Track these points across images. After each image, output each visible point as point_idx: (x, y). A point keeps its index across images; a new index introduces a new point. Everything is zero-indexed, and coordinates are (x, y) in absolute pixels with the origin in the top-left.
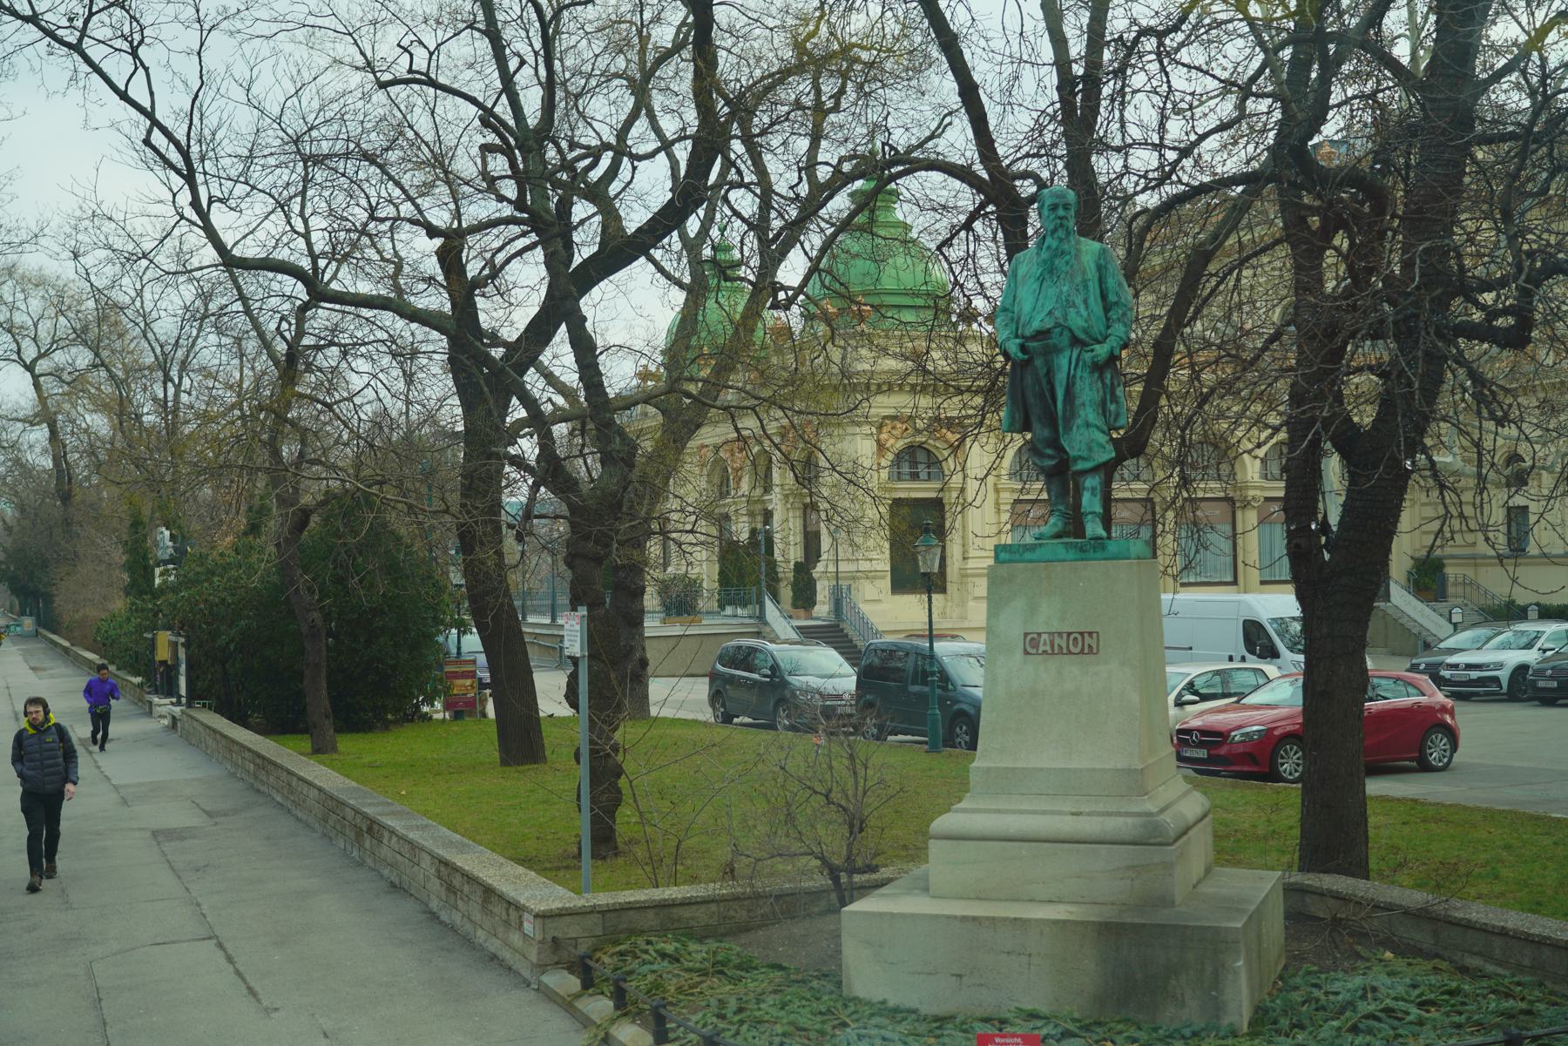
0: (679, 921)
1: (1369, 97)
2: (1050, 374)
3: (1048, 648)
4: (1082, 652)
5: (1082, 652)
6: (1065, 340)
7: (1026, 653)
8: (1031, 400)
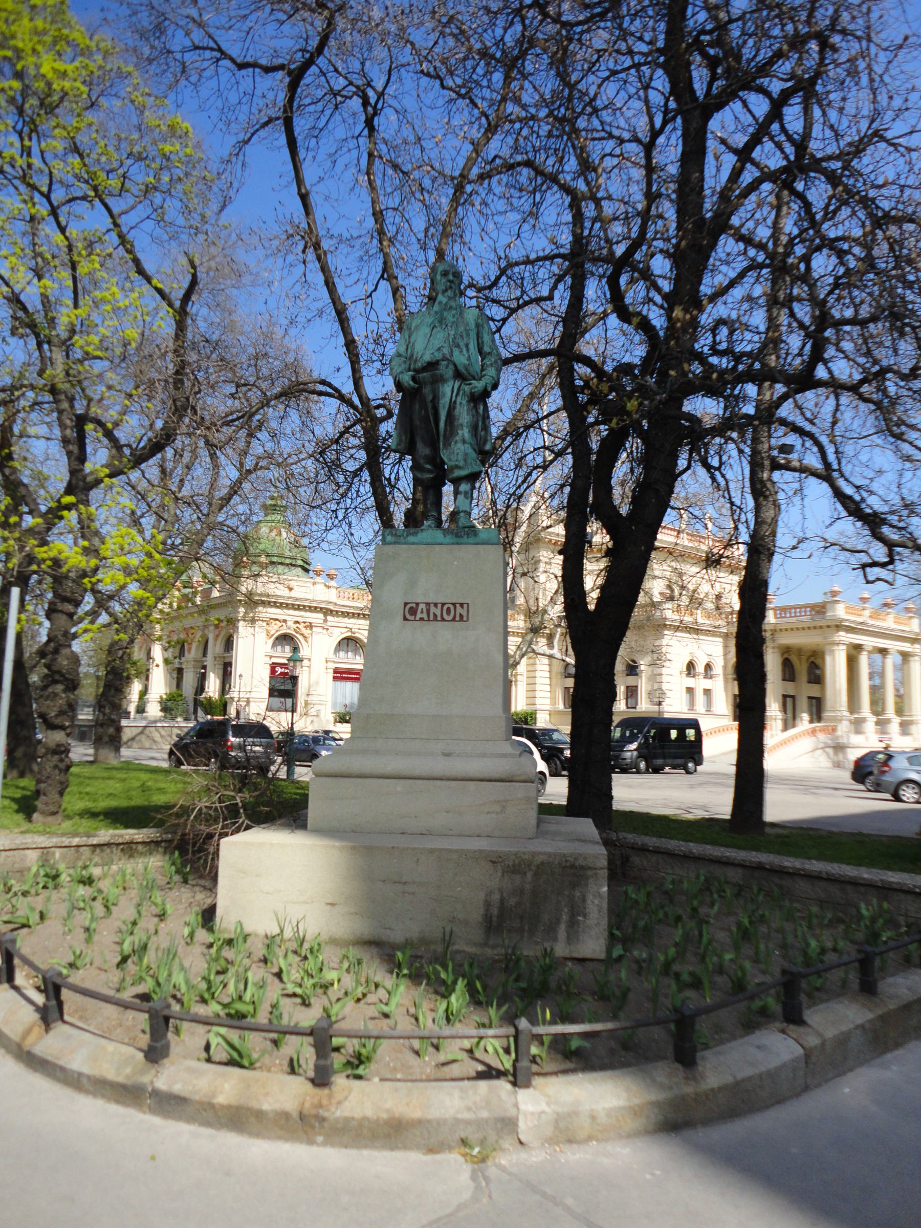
3: (425, 616)
4: (454, 620)
5: (454, 620)
6: (450, 372)
7: (405, 619)
8: (417, 422)
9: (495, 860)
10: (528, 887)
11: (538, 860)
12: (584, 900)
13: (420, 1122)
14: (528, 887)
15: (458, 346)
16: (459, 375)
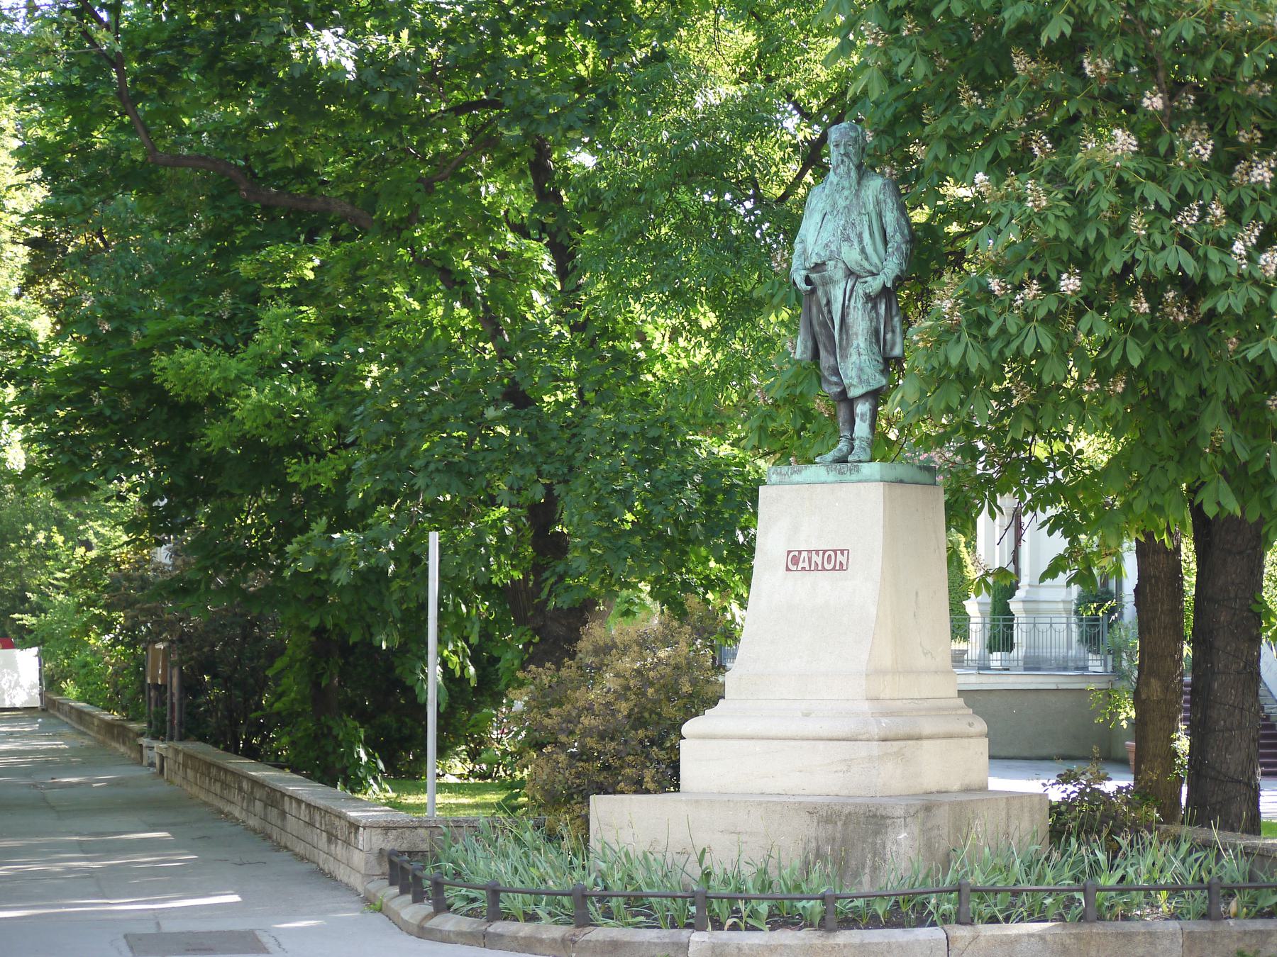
0: (1257, 602)
1: (264, 450)
4: (834, 569)
5: (834, 569)
6: (839, 274)
7: (788, 569)
8: (817, 328)
9: (812, 811)
10: (838, 835)
11: (847, 810)
12: (884, 848)
13: (628, 943)
14: (838, 835)
15: (848, 239)
16: (850, 273)
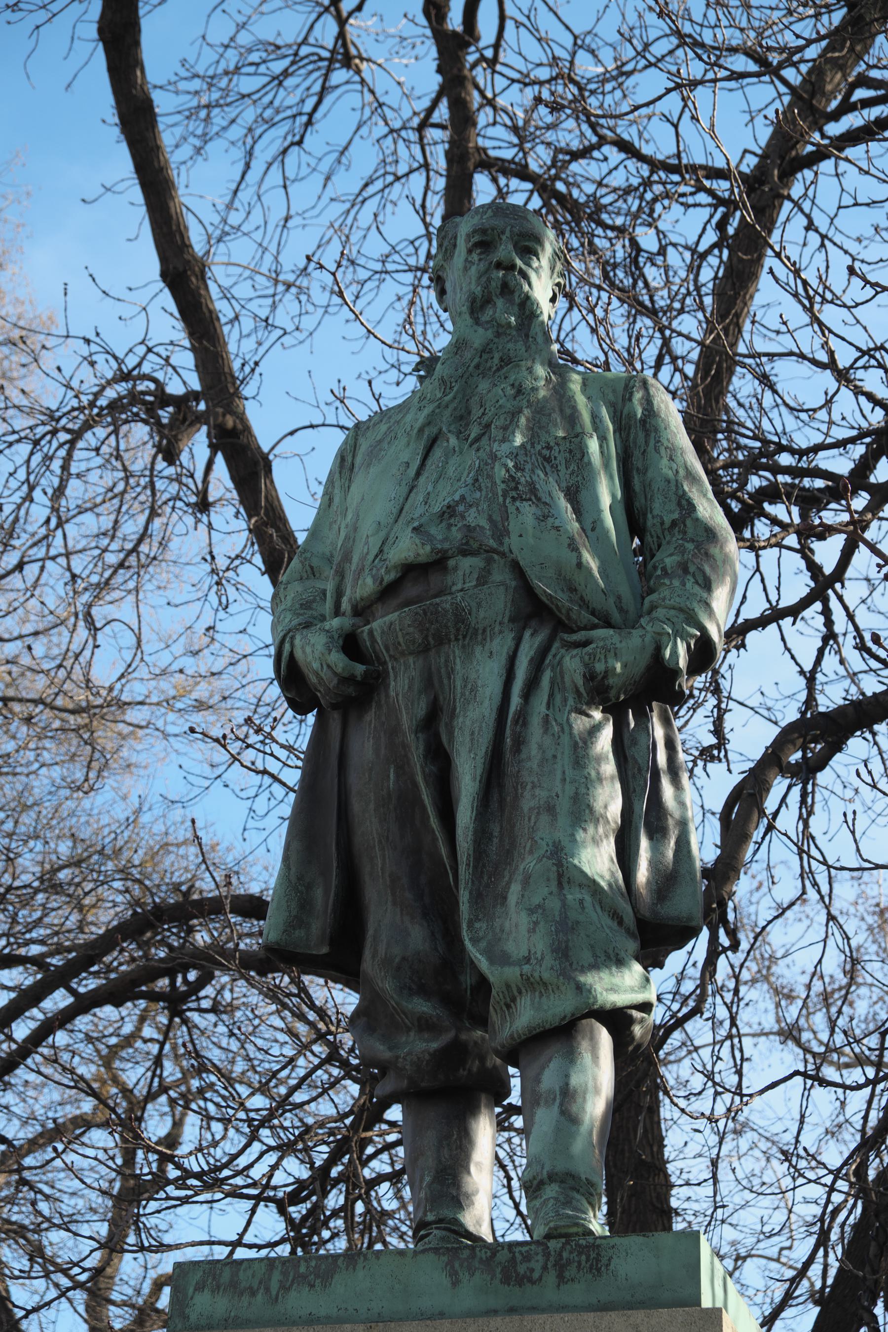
2: (435, 721)
6: (496, 603)
